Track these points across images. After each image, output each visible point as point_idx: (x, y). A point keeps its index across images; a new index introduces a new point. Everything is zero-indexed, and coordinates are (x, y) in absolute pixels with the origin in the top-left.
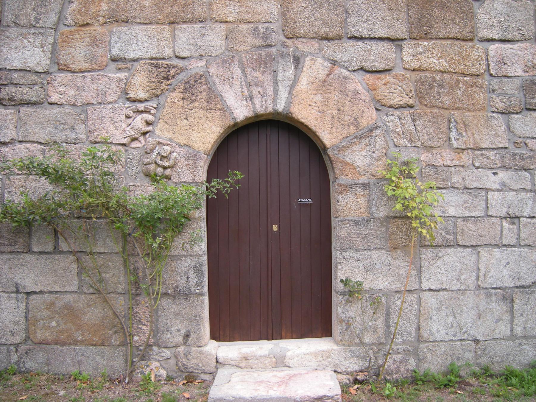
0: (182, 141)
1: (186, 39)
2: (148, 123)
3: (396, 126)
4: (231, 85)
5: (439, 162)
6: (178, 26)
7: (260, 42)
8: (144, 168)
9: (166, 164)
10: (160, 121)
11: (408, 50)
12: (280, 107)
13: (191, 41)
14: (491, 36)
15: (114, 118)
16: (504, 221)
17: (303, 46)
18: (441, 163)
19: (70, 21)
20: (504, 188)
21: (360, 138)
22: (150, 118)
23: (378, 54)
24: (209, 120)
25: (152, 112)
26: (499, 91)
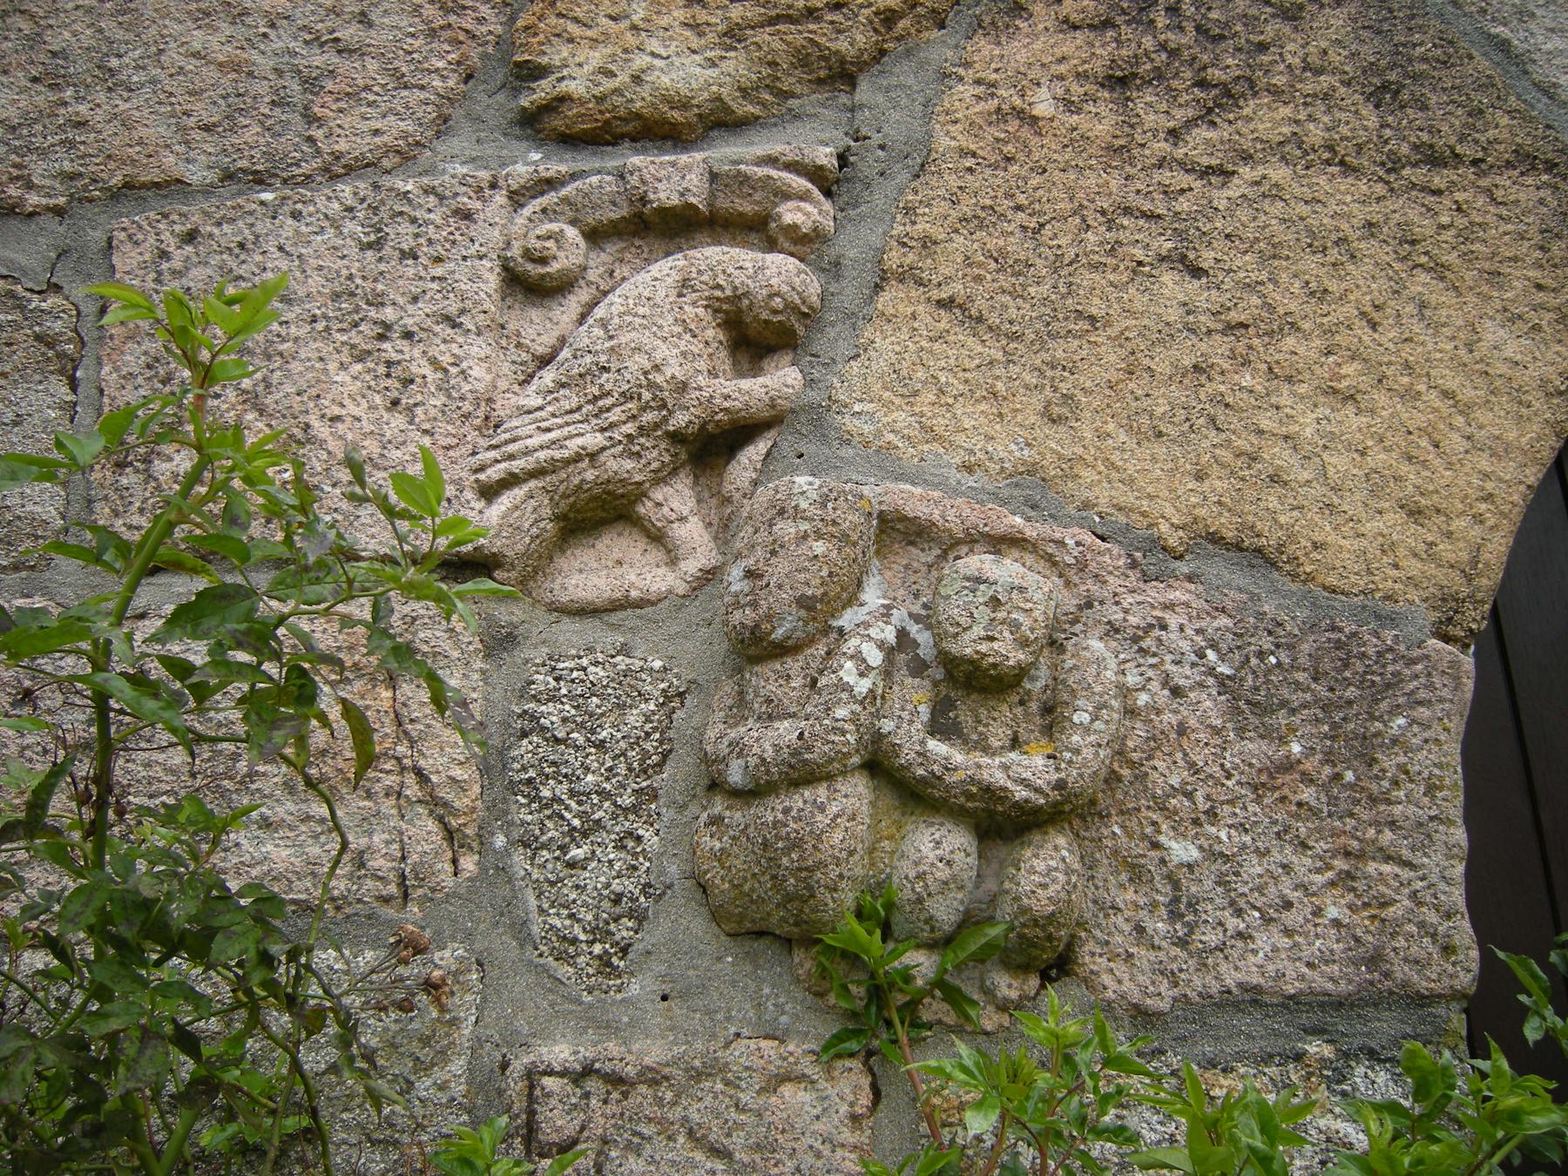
0: (1169, 498)
2: (752, 336)
8: (724, 834)
9: (1025, 771)
10: (884, 300)
15: (377, 301)
22: (773, 273)
24: (1439, 270)
25: (791, 214)
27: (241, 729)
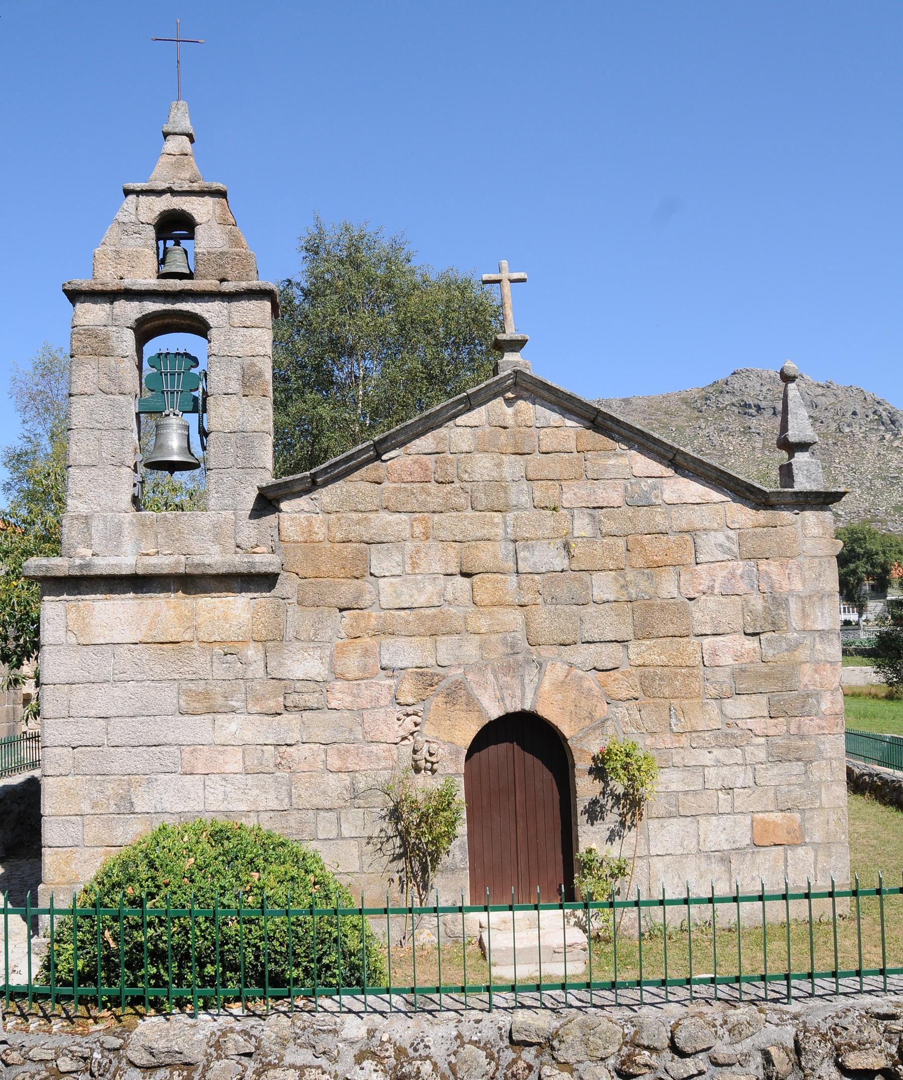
1: (446, 649)
2: (416, 725)
3: (624, 717)
4: (485, 689)
5: (661, 745)
6: (438, 638)
7: (509, 651)
11: (633, 648)
12: (527, 707)
13: (451, 652)
14: (704, 632)
16: (720, 792)
17: (547, 652)
18: (663, 746)
19: (343, 635)
20: (719, 764)
21: (594, 729)
22: (418, 720)
23: (608, 655)
26: (713, 680)
27: (374, 925)
